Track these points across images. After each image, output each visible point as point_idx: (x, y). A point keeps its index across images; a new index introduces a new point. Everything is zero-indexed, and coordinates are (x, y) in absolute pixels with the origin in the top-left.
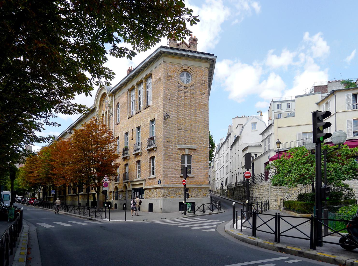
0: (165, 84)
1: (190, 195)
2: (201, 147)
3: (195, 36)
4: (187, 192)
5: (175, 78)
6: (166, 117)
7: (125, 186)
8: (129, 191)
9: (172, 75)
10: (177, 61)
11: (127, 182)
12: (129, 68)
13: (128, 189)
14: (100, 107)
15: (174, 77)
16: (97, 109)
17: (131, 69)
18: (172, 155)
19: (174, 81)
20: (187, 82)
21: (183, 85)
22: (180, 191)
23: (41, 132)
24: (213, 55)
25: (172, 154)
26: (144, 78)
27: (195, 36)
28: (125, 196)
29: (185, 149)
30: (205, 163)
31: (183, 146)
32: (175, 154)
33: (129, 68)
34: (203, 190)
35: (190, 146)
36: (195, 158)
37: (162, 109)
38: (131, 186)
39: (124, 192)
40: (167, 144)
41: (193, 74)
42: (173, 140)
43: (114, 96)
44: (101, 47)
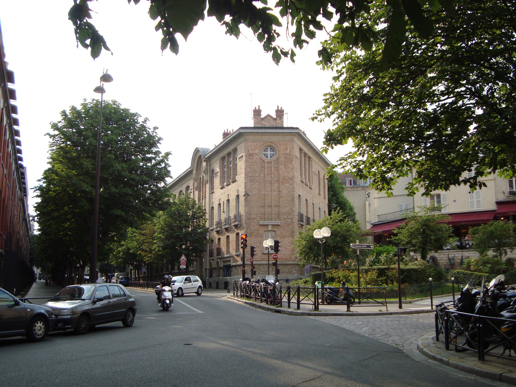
0: (246, 162)
1: (257, 273)
2: (286, 222)
3: (281, 108)
4: (254, 270)
5: (257, 155)
6: (246, 195)
7: (218, 262)
8: (221, 267)
9: (254, 152)
10: (258, 137)
11: (219, 258)
12: (225, 131)
13: (220, 266)
14: (197, 170)
15: (255, 154)
16: (194, 172)
17: (226, 132)
18: (254, 232)
19: (256, 158)
20: (271, 157)
21: (266, 161)
22: (262, 268)
23: (157, 129)
24: (297, 128)
25: (254, 231)
26: (232, 150)
27: (281, 108)
28: (218, 273)
29: (268, 225)
30: (291, 238)
31: (266, 223)
32: (258, 230)
33: (225, 131)
34: (289, 267)
35: (274, 222)
36: (279, 233)
37: (244, 186)
38: (222, 263)
39: (217, 269)
40: (249, 221)
41: (277, 148)
42: (254, 217)
43: (210, 161)
44: (86, 320)
